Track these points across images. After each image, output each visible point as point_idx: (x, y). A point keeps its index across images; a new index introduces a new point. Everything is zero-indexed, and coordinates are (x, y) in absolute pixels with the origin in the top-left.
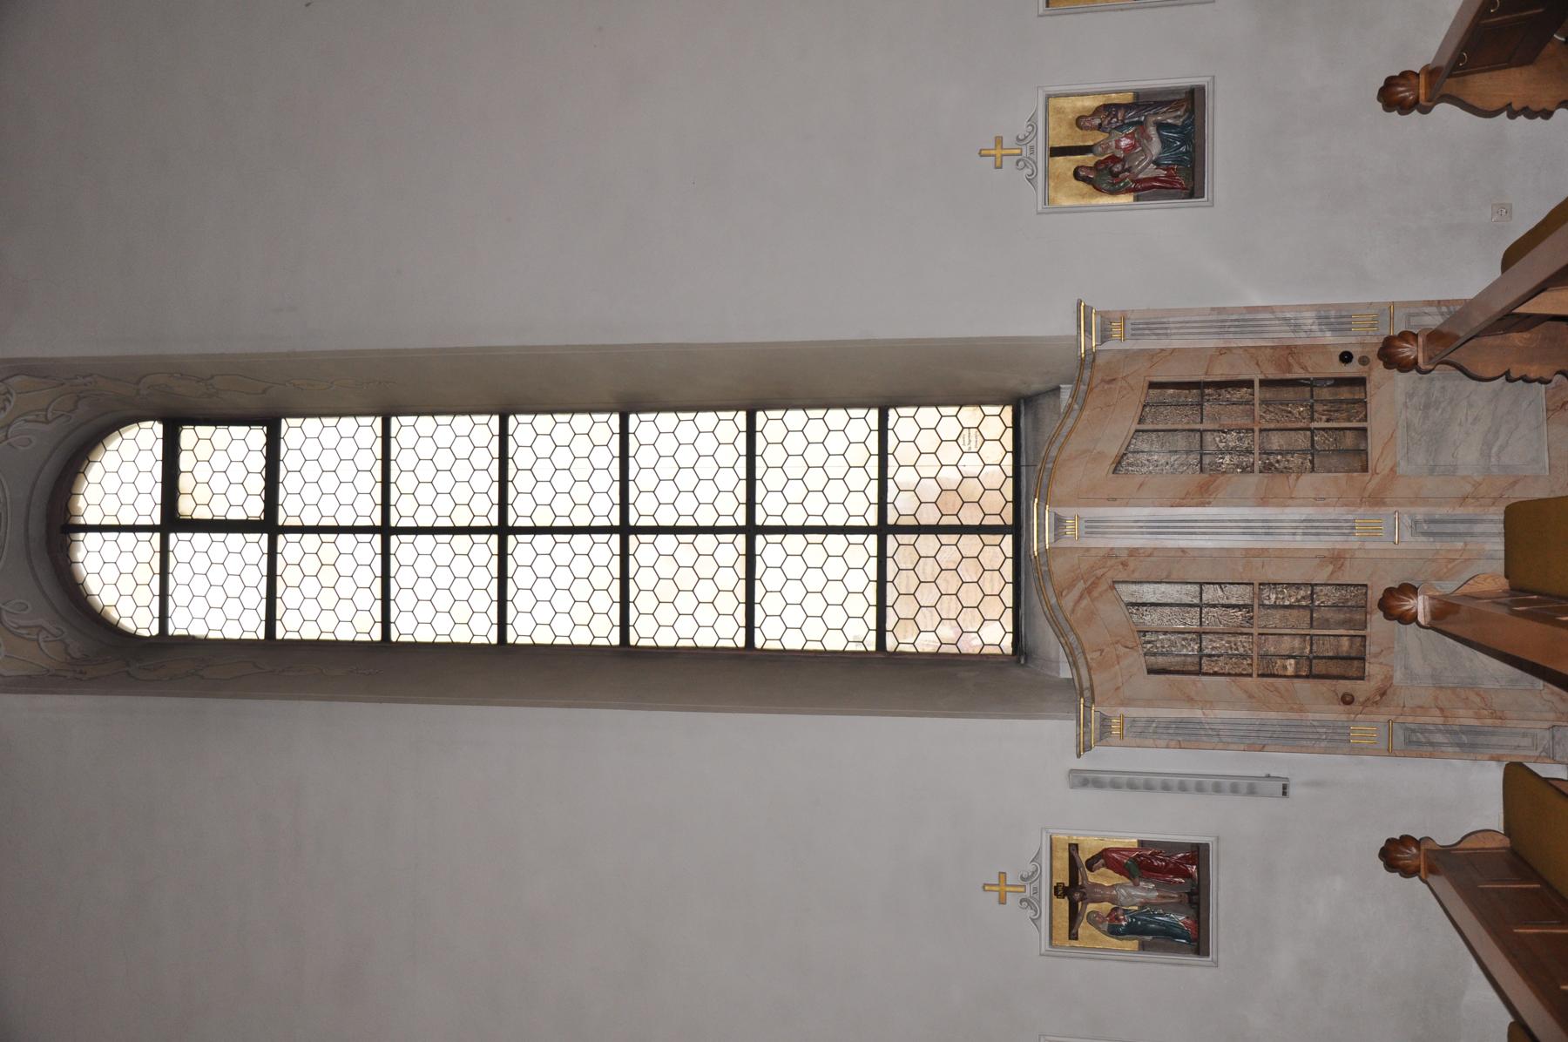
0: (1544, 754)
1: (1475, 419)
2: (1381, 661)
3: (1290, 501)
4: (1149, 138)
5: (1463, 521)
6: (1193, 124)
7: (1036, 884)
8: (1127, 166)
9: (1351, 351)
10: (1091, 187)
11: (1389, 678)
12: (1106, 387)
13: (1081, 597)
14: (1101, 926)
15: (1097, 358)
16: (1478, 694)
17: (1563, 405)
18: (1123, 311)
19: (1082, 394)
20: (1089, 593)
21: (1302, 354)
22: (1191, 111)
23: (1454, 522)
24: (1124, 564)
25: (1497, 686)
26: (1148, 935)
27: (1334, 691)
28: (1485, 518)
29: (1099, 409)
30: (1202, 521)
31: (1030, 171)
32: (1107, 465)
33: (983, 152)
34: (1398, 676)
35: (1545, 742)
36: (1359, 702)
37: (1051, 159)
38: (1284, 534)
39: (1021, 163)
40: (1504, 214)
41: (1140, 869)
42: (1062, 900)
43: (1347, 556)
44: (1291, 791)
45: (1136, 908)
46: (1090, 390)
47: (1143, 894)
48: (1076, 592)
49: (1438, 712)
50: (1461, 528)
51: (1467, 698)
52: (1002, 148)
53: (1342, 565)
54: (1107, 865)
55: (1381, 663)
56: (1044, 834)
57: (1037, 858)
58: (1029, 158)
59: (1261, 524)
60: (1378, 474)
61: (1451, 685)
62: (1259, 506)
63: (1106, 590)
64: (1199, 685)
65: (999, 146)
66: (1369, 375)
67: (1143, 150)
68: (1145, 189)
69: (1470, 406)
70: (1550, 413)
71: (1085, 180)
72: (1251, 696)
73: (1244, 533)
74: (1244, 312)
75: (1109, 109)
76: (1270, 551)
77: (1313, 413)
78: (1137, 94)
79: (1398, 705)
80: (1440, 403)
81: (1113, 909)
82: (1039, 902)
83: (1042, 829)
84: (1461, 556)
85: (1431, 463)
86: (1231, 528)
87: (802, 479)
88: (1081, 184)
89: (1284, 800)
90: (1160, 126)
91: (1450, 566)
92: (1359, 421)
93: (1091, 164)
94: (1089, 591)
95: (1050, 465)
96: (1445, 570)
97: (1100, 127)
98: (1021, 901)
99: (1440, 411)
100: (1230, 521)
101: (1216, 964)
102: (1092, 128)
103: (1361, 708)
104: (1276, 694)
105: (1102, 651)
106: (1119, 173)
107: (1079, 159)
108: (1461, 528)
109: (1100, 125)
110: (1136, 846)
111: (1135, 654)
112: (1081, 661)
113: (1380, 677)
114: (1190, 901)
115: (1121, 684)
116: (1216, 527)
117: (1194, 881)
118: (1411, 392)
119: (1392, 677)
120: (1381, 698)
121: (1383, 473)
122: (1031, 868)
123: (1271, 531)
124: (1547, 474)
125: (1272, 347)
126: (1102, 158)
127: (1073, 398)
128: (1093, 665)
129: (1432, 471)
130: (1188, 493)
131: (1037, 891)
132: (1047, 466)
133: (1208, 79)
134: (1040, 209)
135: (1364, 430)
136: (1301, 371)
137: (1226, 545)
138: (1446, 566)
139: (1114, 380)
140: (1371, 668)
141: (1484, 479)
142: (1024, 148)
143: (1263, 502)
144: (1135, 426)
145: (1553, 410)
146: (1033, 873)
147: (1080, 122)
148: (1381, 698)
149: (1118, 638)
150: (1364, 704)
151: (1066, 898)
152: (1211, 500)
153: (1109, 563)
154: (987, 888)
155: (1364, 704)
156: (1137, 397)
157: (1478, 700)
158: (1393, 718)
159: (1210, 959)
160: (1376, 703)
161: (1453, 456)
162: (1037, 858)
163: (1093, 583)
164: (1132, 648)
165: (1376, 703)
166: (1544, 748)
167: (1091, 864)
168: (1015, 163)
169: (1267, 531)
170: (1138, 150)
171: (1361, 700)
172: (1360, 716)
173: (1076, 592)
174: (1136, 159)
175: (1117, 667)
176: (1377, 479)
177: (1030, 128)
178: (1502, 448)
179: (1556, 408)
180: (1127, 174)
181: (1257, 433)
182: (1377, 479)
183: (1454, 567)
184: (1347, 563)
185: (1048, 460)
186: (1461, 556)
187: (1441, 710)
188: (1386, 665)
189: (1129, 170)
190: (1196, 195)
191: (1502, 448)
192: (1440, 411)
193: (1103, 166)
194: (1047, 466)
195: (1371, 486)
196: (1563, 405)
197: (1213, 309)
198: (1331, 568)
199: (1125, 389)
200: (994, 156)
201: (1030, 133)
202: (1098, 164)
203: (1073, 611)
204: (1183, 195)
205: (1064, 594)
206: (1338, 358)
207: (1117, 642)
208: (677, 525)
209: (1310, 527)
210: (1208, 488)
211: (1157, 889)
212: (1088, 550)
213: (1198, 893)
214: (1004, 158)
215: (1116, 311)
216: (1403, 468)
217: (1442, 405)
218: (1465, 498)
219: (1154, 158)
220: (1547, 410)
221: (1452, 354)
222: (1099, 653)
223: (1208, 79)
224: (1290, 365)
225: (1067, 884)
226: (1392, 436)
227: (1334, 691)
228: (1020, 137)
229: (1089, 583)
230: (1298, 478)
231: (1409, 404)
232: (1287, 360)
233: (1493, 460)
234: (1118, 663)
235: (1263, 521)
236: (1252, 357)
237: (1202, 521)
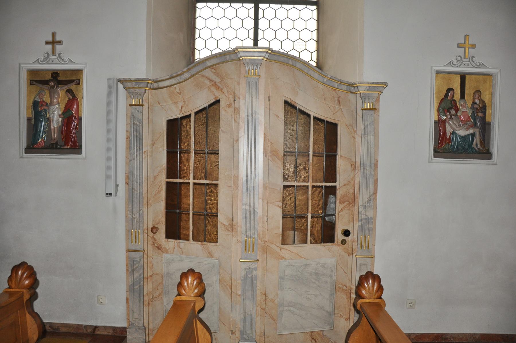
0: (131, 323)
1: (309, 299)
2: (176, 247)
3: (266, 202)
4: (467, 129)
5: (252, 295)
6: (473, 153)
7: (57, 61)
8: (453, 117)
9: (350, 237)
10: (443, 97)
11: (167, 251)
12: (336, 99)
13: (211, 80)
14: (37, 97)
15: (352, 94)
16: (160, 294)
17: (314, 339)
18: (379, 110)
19: (332, 84)
20: (213, 85)
21: (349, 209)
22: (479, 152)
23: (252, 290)
24: (230, 105)
25: (165, 304)
26: (35, 121)
27: (159, 222)
28: (254, 306)
29: (323, 94)
30: (255, 152)
31: (455, 63)
32: (291, 98)
33: (467, 37)
34: (168, 256)
35: (137, 324)
36: (154, 236)
37: (459, 76)
38: (246, 198)
39: (459, 58)
40: (410, 305)
41: (68, 117)
42: (50, 76)
43: (233, 233)
44: (110, 199)
45: (48, 116)
46: (334, 89)
47: (55, 119)
48: (213, 77)
49: (150, 274)
50: (249, 294)
51: (157, 289)
52: (469, 48)
53: (228, 230)
54: (69, 99)
55: (174, 248)
56: (84, 66)
57: (71, 61)
58: (462, 63)
59: (252, 185)
60: (281, 250)
61: (164, 282)
62: (264, 184)
63: (214, 95)
64: (161, 149)
65: (470, 46)
66: (335, 245)
67: (461, 126)
68: (440, 125)
69: (316, 296)
70: (310, 333)
71: (446, 95)
72: (155, 178)
73: (247, 176)
74: (375, 178)
75: (483, 109)
76: (237, 191)
77: (317, 217)
78: (489, 124)
79: (153, 255)
80: (318, 281)
81: (47, 103)
82: (48, 63)
83: (87, 64)
84: (233, 292)
85: (286, 278)
86: (251, 169)
87: (269, 27)
88: (445, 92)
89: (105, 194)
90: (473, 135)
91: (227, 286)
92: (311, 240)
93: (455, 98)
94: (215, 85)
95: (291, 63)
96: (225, 284)
97: (474, 103)
98: (48, 53)
99: (314, 281)
100: (255, 168)
101: (22, 157)
102: (474, 99)
103: (151, 236)
104: (157, 192)
105: (180, 93)
106: (450, 113)
107: (458, 91)
108: (249, 294)
109: (476, 103)
110: (79, 116)
111: (178, 113)
112: (173, 81)
113: (167, 247)
114: (52, 144)
115: (161, 105)
116: (251, 159)
117: (64, 146)
118: (325, 266)
119: (167, 253)
120: (157, 247)
121: (281, 253)
122: (66, 58)
123: (249, 191)
124: (277, 334)
125: (354, 193)
126: (457, 104)
127: (330, 78)
128: (172, 88)
129: (282, 278)
130: (272, 143)
131: (53, 62)
132: (290, 60)
133: (496, 161)
134: (434, 68)
135: (306, 243)
136: (340, 209)
137: (241, 165)
138: (227, 285)
139: (340, 104)
140: (172, 242)
141: (276, 304)
142: (467, 60)
143: (266, 187)
144: (312, 115)
145: (311, 335)
146: (63, 60)
147: (478, 92)
148: (157, 247)
149: (187, 103)
150: (153, 238)
151: (52, 78)
152: (268, 157)
153: (231, 97)
155: (153, 238)
156: (329, 117)
157: (157, 294)
158: (146, 252)
159: (24, 154)
160: (154, 244)
161: (289, 288)
162: (71, 61)
163: (219, 87)
164: (181, 110)
165: (154, 244)
166: (134, 324)
167: (69, 91)
168: (460, 55)
169: (249, 189)
170: (461, 124)
171: (155, 236)
172: (146, 235)
173: (213, 77)
174: (457, 121)
175: (171, 102)
176: (278, 250)
177: (479, 64)
178: (292, 312)
179: (313, 336)
180: (449, 117)
181: (310, 189)
182: (278, 250)
183: (227, 288)
184: (230, 233)
185: (294, 62)
186: (233, 292)
187: (152, 276)
188: (174, 250)
189: (451, 118)
190: (435, 153)
191: (292, 312)
192: (314, 281)
193: (453, 104)
194: (290, 60)
195: (273, 247)
196: (314, 339)
197: (377, 161)
198: (227, 224)
199: (334, 109)
200: (465, 43)
201: (476, 64)
202: (455, 102)
203: (203, 76)
204: (435, 147)
205: (212, 70)
206: (346, 229)
207: (184, 102)
208: (253, 19)
209: (251, 177)
210: (275, 156)
211: (59, 127)
212: (239, 84)
213: (56, 148)
214: (463, 49)
215: (379, 106)
216: (284, 263)
217: (317, 282)
218: (265, 295)
219: (456, 132)
220: (311, 332)
221: (366, 320)
222: (179, 92)
223: (496, 161)
224: (344, 202)
225: (59, 79)
226: (301, 257)
227: (159, 222)
228: (474, 58)
229: (219, 85)
230: (280, 207)
231: (319, 265)
232: (346, 201)
233: (287, 308)
234: (173, 103)
235: (254, 187)
236: (349, 182)
237: (255, 152)
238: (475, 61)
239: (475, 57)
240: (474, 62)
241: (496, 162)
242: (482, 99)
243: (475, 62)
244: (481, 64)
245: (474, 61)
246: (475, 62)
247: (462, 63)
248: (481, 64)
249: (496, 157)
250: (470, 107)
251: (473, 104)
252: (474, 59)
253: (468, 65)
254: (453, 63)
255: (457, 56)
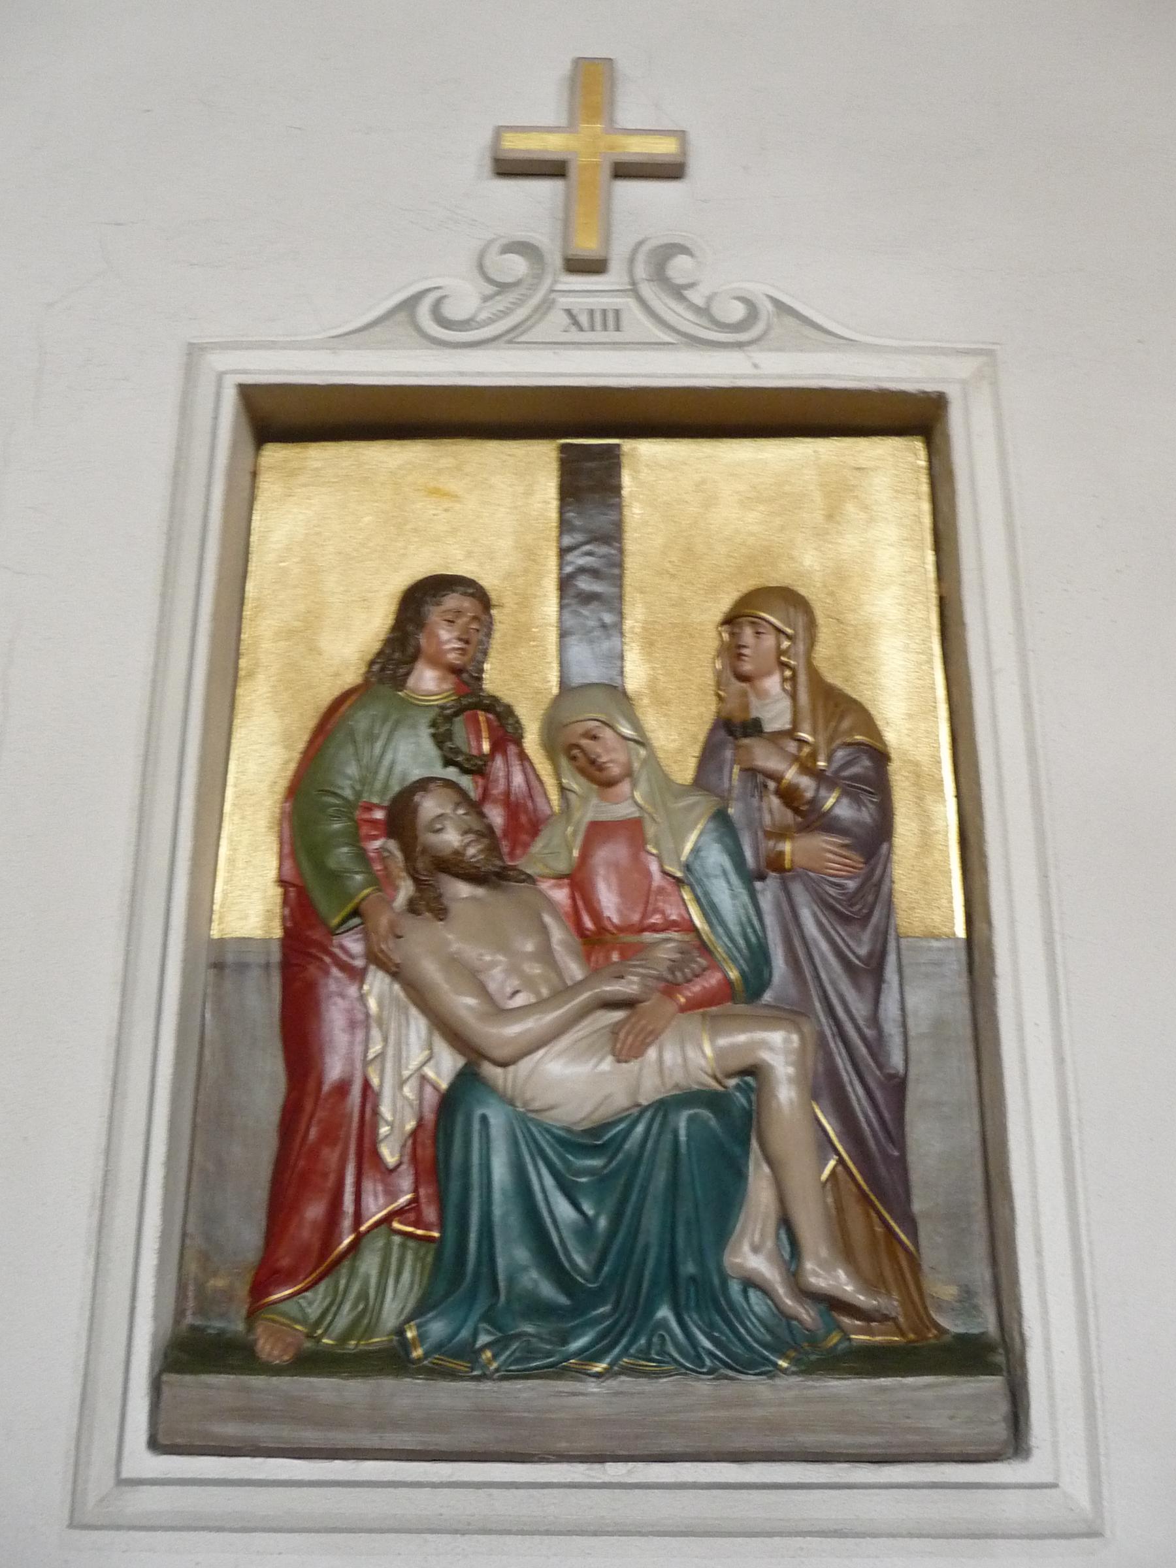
39: (518, 266)
83: (990, 353)
109: (753, 728)
133: (1076, 1487)
134: (219, 361)
154: (664, 148)
168: (521, 235)
177: (737, 312)
201: (704, 312)
238: (692, 285)
239: (684, 250)
240: (678, 292)
241: (1083, 1498)
242: (833, 678)
243: (690, 294)
244: (766, 307)
245: (680, 280)
246: (696, 297)
247: (546, 306)
248: (766, 307)
249: (1072, 1426)
250: (684, 771)
251: (722, 734)
252: (679, 269)
253: (613, 319)
254: (451, 311)
255: (495, 248)
